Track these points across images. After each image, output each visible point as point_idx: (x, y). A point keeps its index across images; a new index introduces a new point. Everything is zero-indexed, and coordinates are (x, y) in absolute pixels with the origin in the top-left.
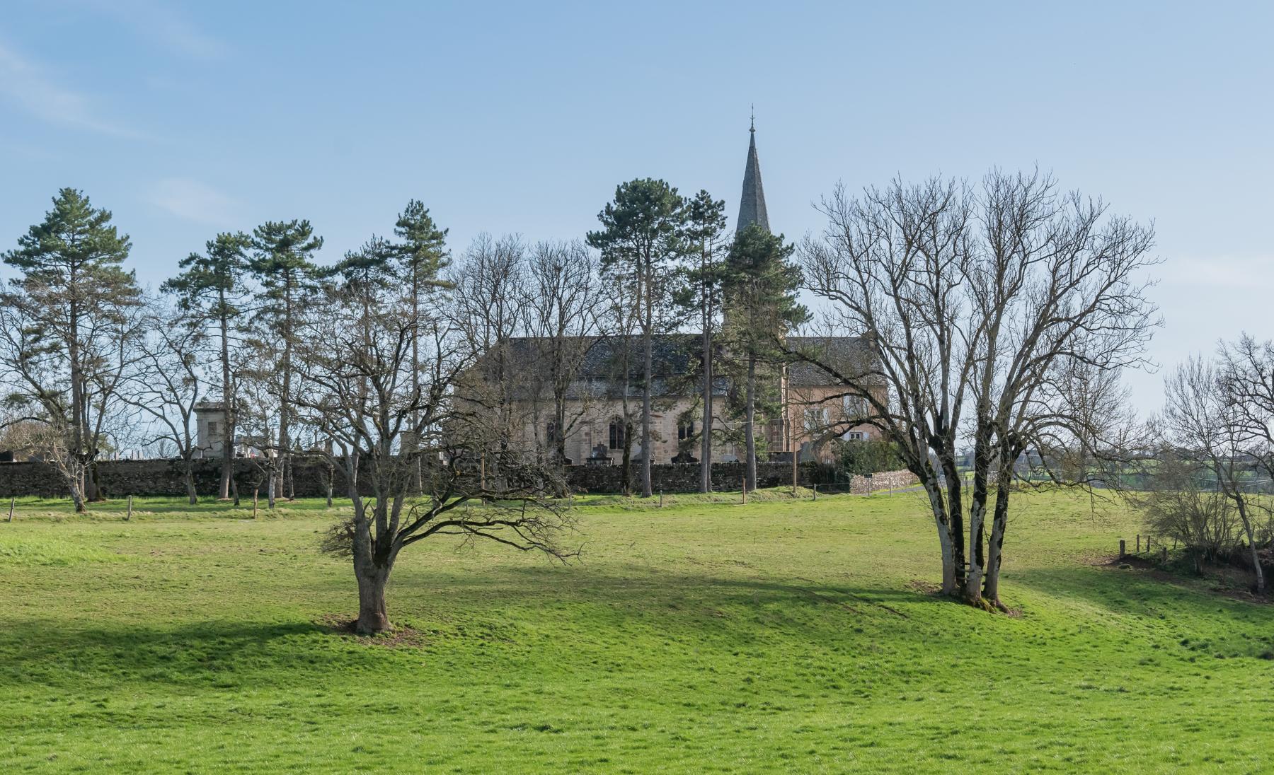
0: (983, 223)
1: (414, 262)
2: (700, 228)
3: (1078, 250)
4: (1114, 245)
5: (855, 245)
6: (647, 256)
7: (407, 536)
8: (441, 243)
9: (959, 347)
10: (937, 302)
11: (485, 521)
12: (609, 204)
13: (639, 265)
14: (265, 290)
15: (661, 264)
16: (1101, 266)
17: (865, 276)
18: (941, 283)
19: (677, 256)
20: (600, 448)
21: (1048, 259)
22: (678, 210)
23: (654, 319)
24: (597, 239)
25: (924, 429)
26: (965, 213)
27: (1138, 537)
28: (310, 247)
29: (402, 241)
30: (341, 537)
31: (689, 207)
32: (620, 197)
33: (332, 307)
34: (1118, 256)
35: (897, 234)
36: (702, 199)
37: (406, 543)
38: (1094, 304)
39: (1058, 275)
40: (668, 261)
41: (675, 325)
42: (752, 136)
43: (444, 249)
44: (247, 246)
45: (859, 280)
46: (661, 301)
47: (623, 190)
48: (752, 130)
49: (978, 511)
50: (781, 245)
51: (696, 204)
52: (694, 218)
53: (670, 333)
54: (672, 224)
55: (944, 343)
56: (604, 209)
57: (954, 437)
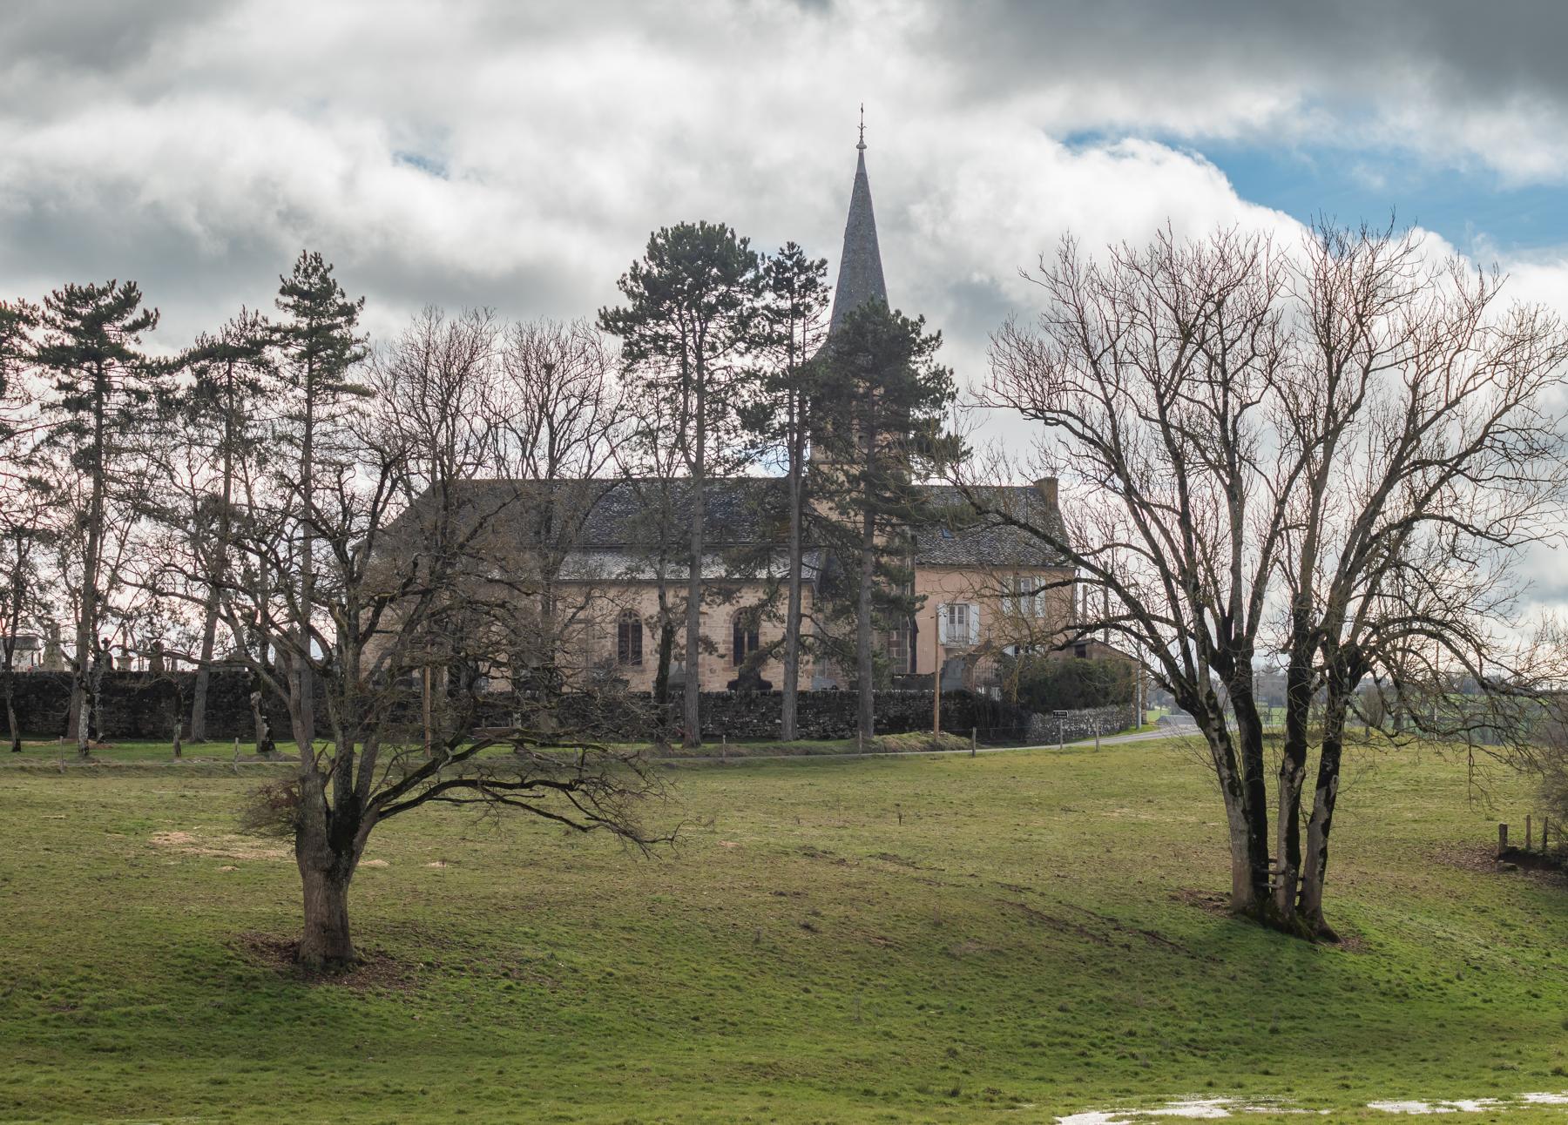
0: (1303, 306)
1: (308, 354)
2: (785, 304)
3: (1459, 351)
4: (1516, 343)
5: (1093, 339)
6: (699, 348)
7: (388, 806)
8: (350, 322)
9: (1259, 501)
10: (1224, 430)
11: (518, 780)
12: (636, 264)
13: (684, 364)
14: (61, 396)
15: (721, 362)
16: (1496, 378)
17: (1111, 389)
18: (1230, 400)
19: (748, 350)
20: (606, 665)
21: (1403, 365)
22: (750, 275)
23: (710, 454)
24: (616, 321)
25: (1203, 637)
26: (1270, 287)
27: (1528, 819)
28: (136, 326)
29: (288, 319)
30: (275, 805)
31: (768, 270)
32: (654, 251)
33: (169, 425)
34: (1522, 364)
35: (1165, 322)
36: (790, 257)
37: (383, 815)
38: (1481, 441)
39: (1421, 391)
40: (735, 356)
41: (740, 463)
42: (861, 155)
43: (356, 332)
44: (32, 323)
45: (1100, 393)
46: (721, 423)
47: (660, 241)
48: (861, 147)
49: (1291, 777)
50: (918, 334)
51: (778, 264)
52: (776, 288)
53: (733, 476)
54: (740, 296)
55: (1236, 495)
56: (628, 271)
57: (1251, 653)
